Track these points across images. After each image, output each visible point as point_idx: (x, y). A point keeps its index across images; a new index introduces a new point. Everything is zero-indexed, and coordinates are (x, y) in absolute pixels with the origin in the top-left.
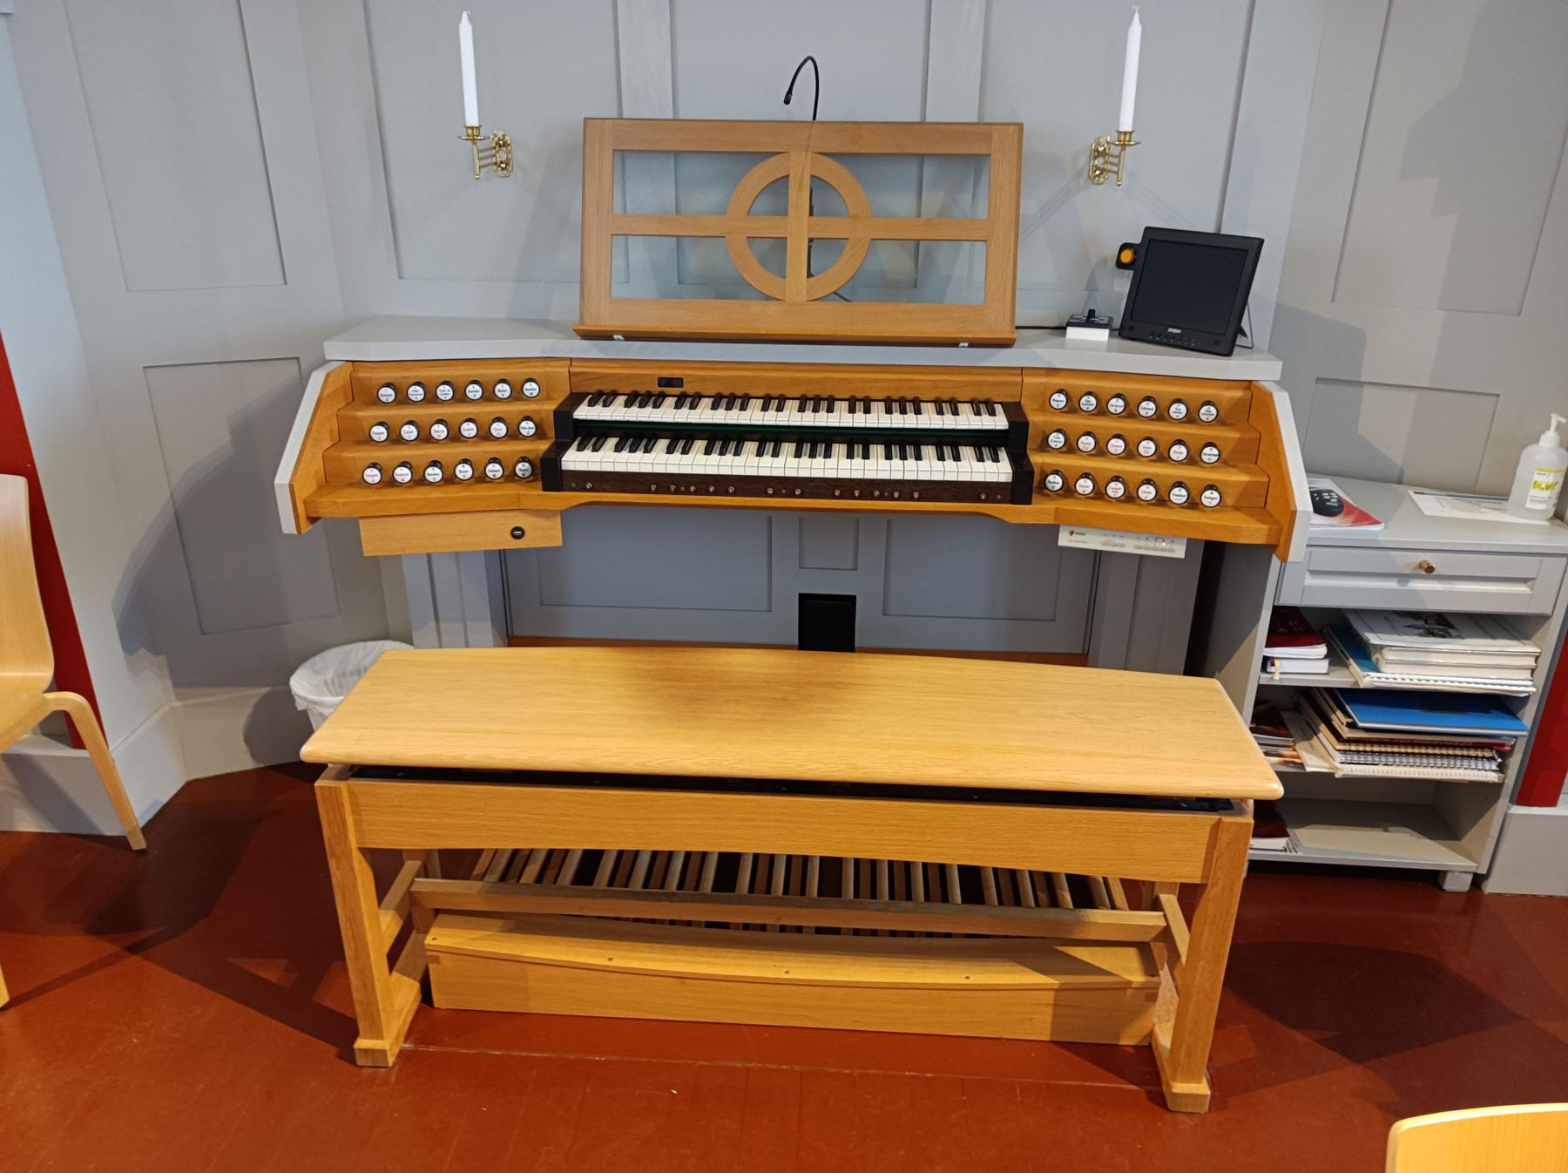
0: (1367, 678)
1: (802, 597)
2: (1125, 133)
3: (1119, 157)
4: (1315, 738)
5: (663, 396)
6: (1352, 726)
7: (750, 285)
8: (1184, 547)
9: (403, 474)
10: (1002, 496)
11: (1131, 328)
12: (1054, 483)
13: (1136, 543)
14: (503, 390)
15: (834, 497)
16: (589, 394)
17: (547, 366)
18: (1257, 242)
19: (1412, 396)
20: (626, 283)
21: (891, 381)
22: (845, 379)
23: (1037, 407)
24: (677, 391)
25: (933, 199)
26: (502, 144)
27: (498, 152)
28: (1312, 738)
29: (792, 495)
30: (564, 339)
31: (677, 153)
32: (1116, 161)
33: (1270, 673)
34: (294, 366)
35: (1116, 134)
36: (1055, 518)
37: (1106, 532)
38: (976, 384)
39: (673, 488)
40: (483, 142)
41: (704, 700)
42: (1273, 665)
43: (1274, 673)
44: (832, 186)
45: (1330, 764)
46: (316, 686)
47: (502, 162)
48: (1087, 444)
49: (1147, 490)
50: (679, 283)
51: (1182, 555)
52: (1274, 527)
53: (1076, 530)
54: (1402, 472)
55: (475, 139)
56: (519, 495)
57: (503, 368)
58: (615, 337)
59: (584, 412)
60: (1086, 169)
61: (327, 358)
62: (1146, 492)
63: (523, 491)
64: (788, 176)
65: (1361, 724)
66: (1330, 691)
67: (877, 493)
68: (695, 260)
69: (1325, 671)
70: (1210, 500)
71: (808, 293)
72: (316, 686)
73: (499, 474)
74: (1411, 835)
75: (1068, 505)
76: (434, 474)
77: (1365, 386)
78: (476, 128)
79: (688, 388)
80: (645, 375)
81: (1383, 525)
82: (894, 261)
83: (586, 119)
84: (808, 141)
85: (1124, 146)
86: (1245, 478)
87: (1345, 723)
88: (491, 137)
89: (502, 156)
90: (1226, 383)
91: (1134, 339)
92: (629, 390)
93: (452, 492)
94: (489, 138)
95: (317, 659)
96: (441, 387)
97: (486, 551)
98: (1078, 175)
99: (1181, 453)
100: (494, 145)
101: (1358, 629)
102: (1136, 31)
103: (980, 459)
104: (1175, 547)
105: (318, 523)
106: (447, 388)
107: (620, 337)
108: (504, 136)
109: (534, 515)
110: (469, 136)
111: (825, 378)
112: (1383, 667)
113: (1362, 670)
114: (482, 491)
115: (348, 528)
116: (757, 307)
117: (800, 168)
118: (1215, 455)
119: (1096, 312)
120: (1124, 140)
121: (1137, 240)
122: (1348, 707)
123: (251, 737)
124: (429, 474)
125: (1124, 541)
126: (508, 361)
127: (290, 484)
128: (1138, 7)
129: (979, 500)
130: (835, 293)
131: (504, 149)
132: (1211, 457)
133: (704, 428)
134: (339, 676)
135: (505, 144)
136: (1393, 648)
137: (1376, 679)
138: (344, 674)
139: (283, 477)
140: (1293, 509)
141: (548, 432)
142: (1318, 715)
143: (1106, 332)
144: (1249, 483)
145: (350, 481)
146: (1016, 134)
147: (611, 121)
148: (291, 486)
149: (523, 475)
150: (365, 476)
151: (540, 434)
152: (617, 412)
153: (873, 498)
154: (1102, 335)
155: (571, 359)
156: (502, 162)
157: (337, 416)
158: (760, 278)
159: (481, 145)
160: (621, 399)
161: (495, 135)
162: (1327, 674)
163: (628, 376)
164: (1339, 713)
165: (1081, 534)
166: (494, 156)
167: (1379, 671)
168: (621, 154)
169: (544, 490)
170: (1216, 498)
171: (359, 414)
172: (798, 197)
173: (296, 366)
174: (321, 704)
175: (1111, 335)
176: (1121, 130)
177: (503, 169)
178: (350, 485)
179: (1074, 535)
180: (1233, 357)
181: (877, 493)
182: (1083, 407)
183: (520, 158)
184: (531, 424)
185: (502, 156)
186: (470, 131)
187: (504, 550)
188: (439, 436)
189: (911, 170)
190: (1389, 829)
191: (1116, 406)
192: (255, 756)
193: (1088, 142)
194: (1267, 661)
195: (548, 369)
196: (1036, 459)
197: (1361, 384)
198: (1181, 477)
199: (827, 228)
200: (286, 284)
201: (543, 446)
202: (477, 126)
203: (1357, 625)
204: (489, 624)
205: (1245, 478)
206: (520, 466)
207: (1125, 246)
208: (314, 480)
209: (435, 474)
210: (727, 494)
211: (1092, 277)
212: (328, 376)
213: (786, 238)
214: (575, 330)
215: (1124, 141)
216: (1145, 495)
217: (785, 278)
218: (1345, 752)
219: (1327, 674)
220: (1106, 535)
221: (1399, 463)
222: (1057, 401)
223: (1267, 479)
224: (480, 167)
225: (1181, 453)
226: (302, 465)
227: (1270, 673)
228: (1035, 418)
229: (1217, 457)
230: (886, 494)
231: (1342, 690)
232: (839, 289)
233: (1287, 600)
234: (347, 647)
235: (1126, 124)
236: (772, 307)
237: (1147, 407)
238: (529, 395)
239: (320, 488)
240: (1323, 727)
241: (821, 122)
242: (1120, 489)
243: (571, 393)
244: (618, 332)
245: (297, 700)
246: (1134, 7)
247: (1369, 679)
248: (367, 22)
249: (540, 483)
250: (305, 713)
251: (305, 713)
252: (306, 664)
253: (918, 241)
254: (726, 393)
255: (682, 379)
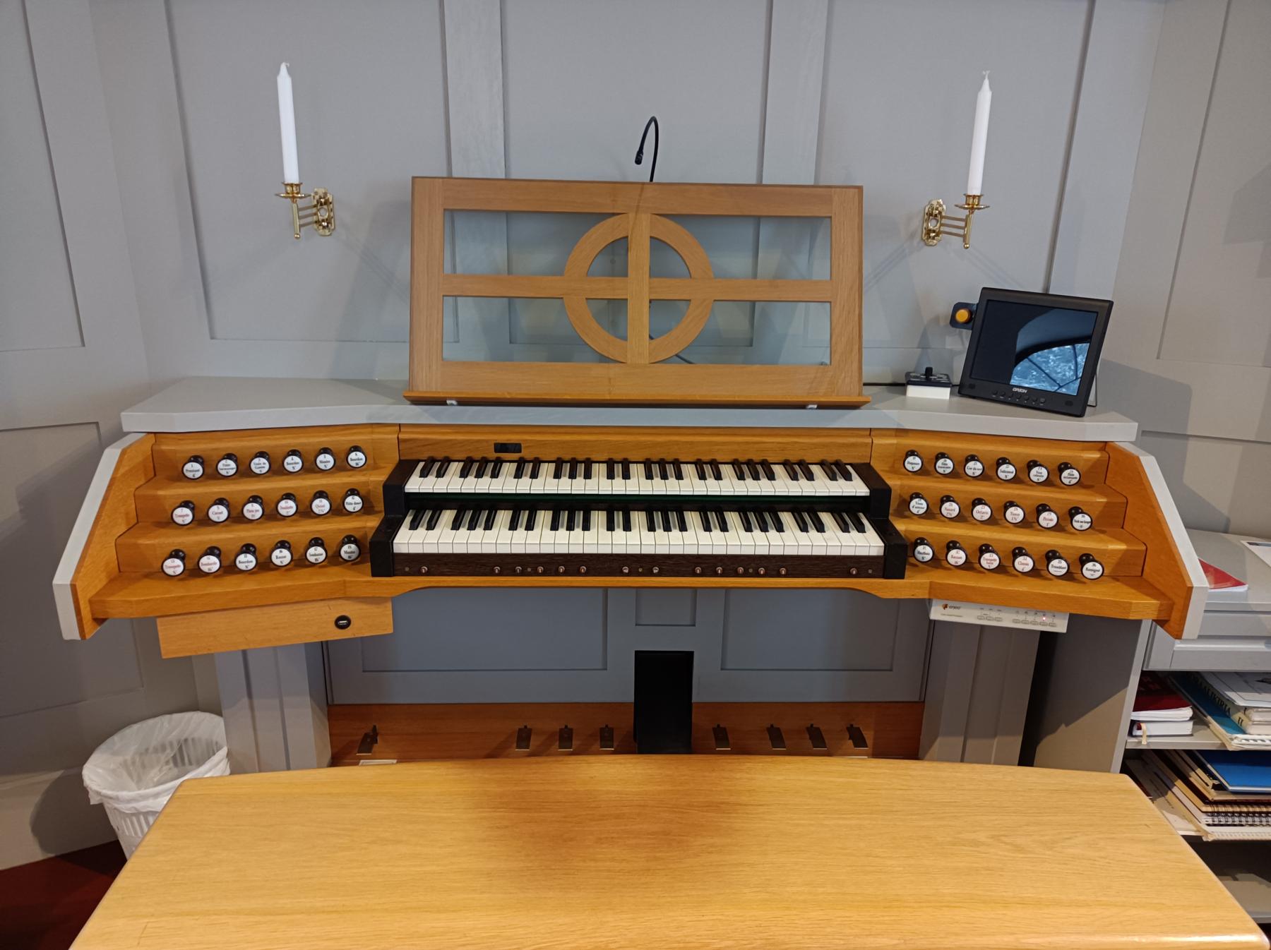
0: (1236, 741)
1: (639, 654)
2: (974, 197)
3: (966, 220)
4: (1170, 792)
5: (499, 463)
6: (1219, 787)
7: (588, 344)
8: (1067, 622)
9: (210, 563)
10: (873, 571)
11: (972, 387)
12: (924, 553)
13: (1015, 616)
14: (326, 461)
15: (695, 575)
16: (419, 461)
17: (372, 433)
18: (1107, 304)
19: (1239, 448)
20: (455, 342)
21: (738, 443)
22: (692, 443)
23: (887, 469)
24: (515, 456)
25: (769, 260)
26: (324, 203)
27: (318, 210)
28: (1166, 793)
29: (650, 573)
30: (394, 404)
31: (508, 214)
32: (962, 224)
33: (1136, 736)
34: (92, 432)
35: (965, 197)
36: (930, 593)
37: (982, 606)
38: (824, 445)
39: (519, 568)
40: (304, 199)
41: (571, 840)
42: (1140, 728)
43: (1141, 736)
44: (669, 245)
45: (1194, 825)
46: (114, 771)
47: (323, 221)
48: (952, 510)
49: (1025, 562)
50: (511, 342)
51: (1064, 630)
52: (1165, 602)
53: (950, 603)
54: (1228, 520)
55: (294, 197)
56: (345, 582)
57: (324, 436)
58: (448, 402)
59: (416, 484)
60: (920, 231)
61: (125, 429)
62: (1023, 564)
63: (349, 576)
64: (627, 237)
65: (1230, 788)
66: (1190, 753)
67: (741, 570)
68: (527, 319)
69: (1189, 733)
70: (1092, 573)
71: (650, 354)
72: (114, 771)
73: (322, 558)
74: (1260, 883)
75: (938, 577)
76: (246, 561)
77: (1191, 438)
78: (297, 185)
79: (525, 453)
80: (478, 441)
81: (1247, 586)
82: (733, 322)
83: (414, 178)
84: (639, 202)
85: (972, 209)
86: (1123, 547)
87: (1211, 785)
88: (313, 194)
89: (323, 214)
90: (1081, 444)
91: (974, 397)
92: (463, 456)
93: (268, 581)
94: (310, 195)
95: (116, 738)
96: (256, 460)
97: (306, 644)
98: (912, 236)
99: (1051, 520)
100: (315, 203)
101: (891, 521)
102: (985, 96)
103: (845, 529)
104: (1056, 621)
105: (106, 623)
106: (263, 460)
107: (454, 402)
108: (325, 194)
109: (362, 602)
110: (288, 193)
111: (670, 441)
112: (1251, 729)
113: (1228, 732)
114: (302, 578)
115: (145, 629)
116: (599, 370)
117: (641, 230)
118: (1088, 523)
119: (933, 370)
120: (972, 204)
121: (974, 299)
122: (1209, 766)
123: (40, 827)
124: (240, 562)
125: (1002, 615)
126: (330, 429)
127: (71, 585)
128: (988, 72)
129: (850, 575)
130: (677, 355)
131: (325, 207)
132: (1084, 524)
133: (548, 498)
134: (141, 754)
135: (327, 203)
136: (1260, 710)
137: (1244, 742)
138: (147, 750)
139: (63, 576)
140: (1189, 585)
141: (375, 504)
142: (1172, 770)
143: (948, 390)
144: (1126, 551)
145: (147, 570)
146: (857, 196)
147: (441, 180)
148: (74, 588)
149: (349, 557)
150: (164, 567)
151: (367, 509)
152: (452, 483)
153: (737, 575)
154: (943, 394)
155: (400, 425)
156: (323, 221)
157: (134, 496)
158: (598, 338)
159: (301, 203)
160: (455, 467)
161: (316, 193)
162: (1191, 735)
163: (462, 442)
164: (1199, 771)
165: (955, 608)
166: (316, 214)
167: (1244, 732)
168: (451, 213)
169: (373, 575)
170: (1099, 571)
171: (161, 493)
172: (640, 255)
173: (95, 431)
174: (117, 799)
175: (952, 393)
176: (970, 193)
177: (324, 227)
178: (147, 576)
179: (948, 609)
180: (1084, 418)
181: (741, 570)
182: (939, 470)
183: (341, 214)
184: (357, 499)
185: (323, 214)
186: (289, 189)
187: (327, 642)
188: (253, 516)
189: (747, 231)
190: (1238, 876)
191: (975, 469)
192: (43, 846)
193: (922, 206)
194: (1135, 724)
195: (375, 436)
196: (901, 526)
197: (1187, 437)
198: (1055, 545)
199: (669, 289)
200: (84, 345)
201: (373, 523)
202: (297, 182)
203: (1217, 686)
204: (308, 698)
205: (1123, 547)
206: (345, 548)
207: (958, 306)
208: (104, 574)
209: (248, 562)
210: (578, 574)
211: (924, 336)
212: (123, 453)
213: (627, 300)
214: (405, 397)
215: (973, 205)
216: (1023, 566)
217: (625, 338)
218: (1212, 814)
219: (1191, 735)
220: (982, 609)
221: (1225, 512)
222: (912, 464)
223: (1144, 548)
224: (301, 226)
225: (1051, 520)
226: (88, 561)
227: (1136, 736)
228: (893, 482)
229: (1090, 524)
230: (751, 571)
231: (1202, 752)
232: (680, 352)
233: (1159, 663)
234: (151, 722)
235: (975, 188)
236: (613, 370)
237: (1006, 470)
238: (355, 465)
239: (112, 581)
240: (1179, 783)
241: (658, 184)
242: (995, 560)
243: (401, 462)
244: (451, 398)
245: (91, 795)
246: (984, 73)
247: (1238, 742)
248: (177, 76)
249: (367, 567)
250: (100, 807)
251: (100, 807)
252: (103, 746)
253: (753, 303)
254: (567, 457)
255: (520, 445)
